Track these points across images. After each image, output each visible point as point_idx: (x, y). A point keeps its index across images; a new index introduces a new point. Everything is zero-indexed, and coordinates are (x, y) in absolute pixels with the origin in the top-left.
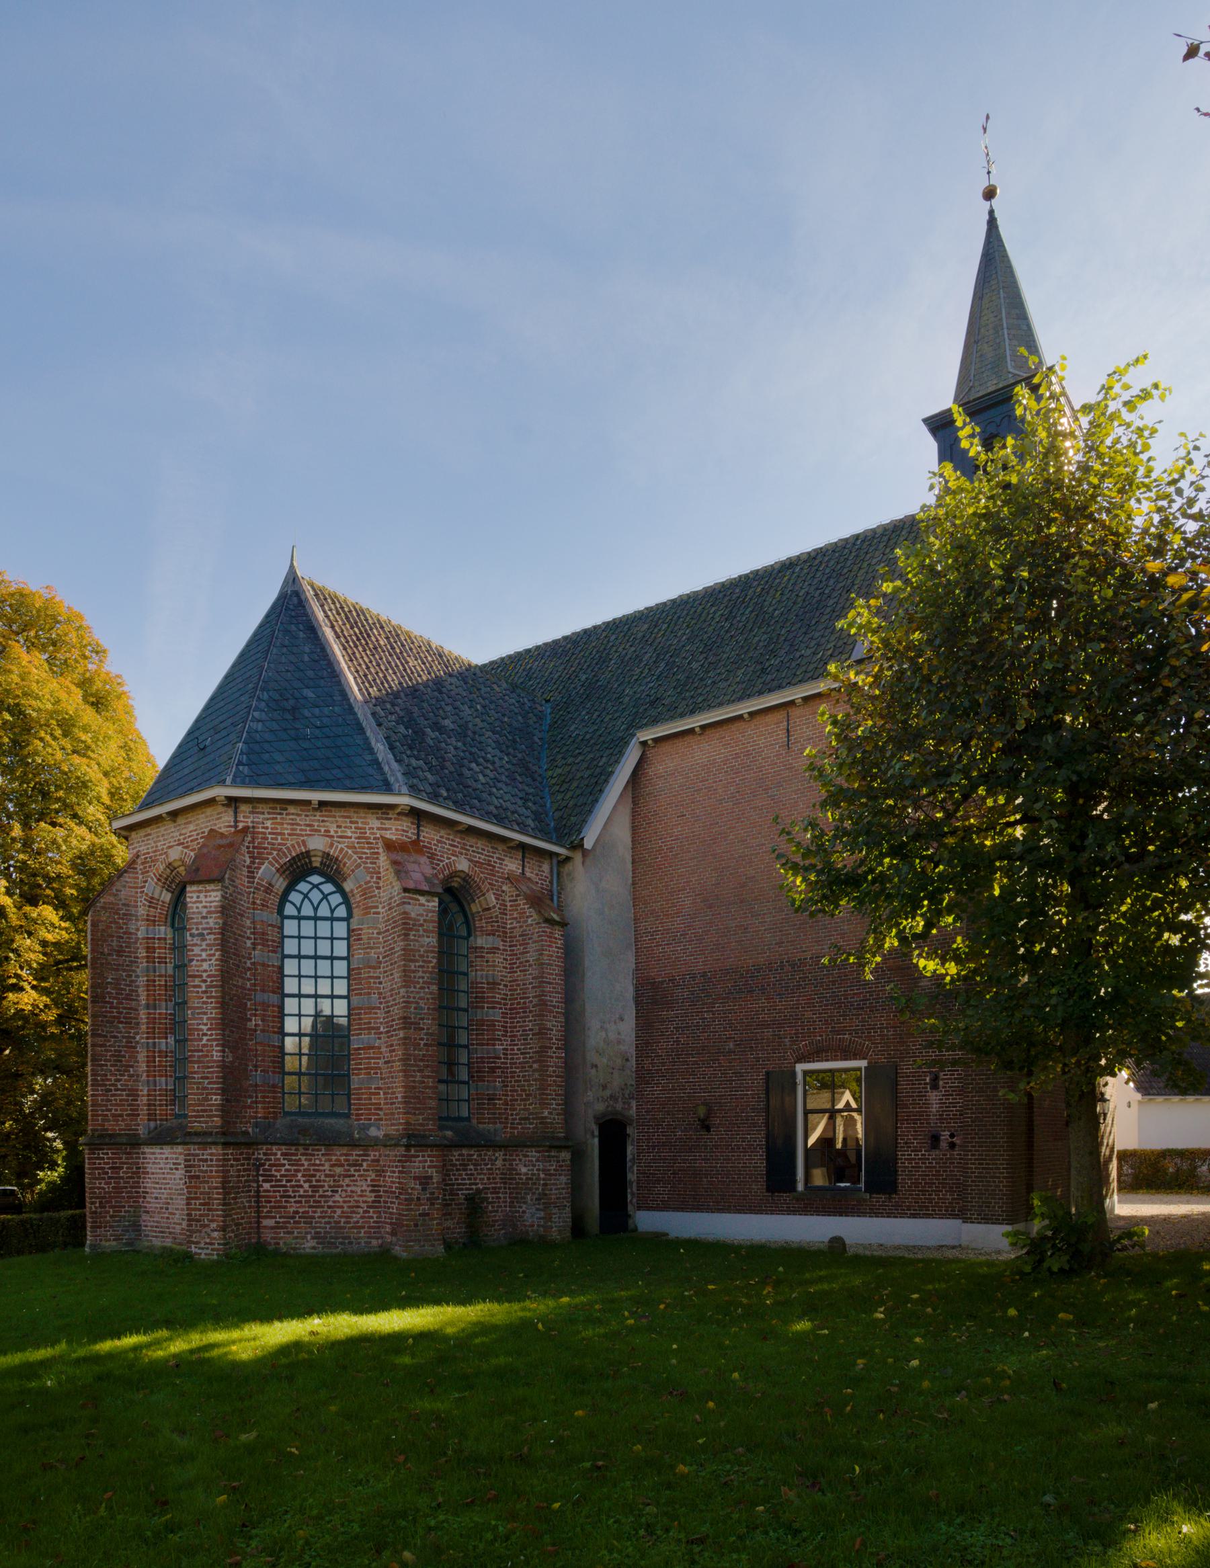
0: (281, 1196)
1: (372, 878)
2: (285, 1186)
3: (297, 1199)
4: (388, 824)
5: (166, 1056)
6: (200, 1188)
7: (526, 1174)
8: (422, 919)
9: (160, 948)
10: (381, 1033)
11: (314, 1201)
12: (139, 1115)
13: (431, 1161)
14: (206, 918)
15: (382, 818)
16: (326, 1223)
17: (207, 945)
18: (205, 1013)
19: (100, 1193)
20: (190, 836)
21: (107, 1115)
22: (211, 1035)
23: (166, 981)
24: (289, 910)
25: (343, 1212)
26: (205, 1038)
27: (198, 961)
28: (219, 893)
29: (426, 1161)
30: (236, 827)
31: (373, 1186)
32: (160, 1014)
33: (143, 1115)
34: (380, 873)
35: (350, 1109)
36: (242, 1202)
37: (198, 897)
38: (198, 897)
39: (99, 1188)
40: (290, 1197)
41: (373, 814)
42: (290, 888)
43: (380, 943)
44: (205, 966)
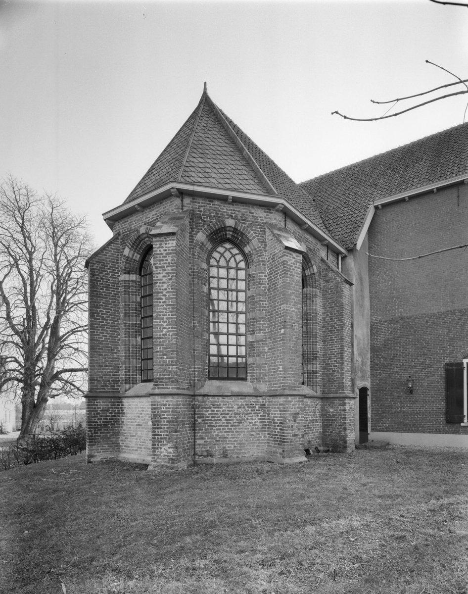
0: (208, 426)
1: (262, 245)
2: (211, 420)
3: (218, 427)
4: (271, 216)
5: (136, 348)
6: (161, 422)
7: (333, 412)
8: (294, 266)
9: (132, 286)
10: (267, 333)
11: (228, 429)
12: (119, 381)
13: (299, 405)
14: (165, 257)
15: (267, 212)
16: (234, 441)
17: (166, 273)
18: (165, 315)
19: (95, 425)
20: (152, 218)
21: (100, 380)
22: (169, 328)
23: (136, 305)
24: (213, 262)
25: (244, 435)
26: (165, 330)
27: (160, 283)
28: (174, 242)
29: (295, 405)
30: (182, 209)
31: (261, 419)
32: (132, 324)
33: (122, 381)
34: (266, 242)
35: (247, 376)
36: (186, 430)
37: (161, 244)
38: (161, 244)
39: (93, 422)
40: (214, 426)
41: (262, 209)
42: (214, 249)
43: (266, 282)
44: (165, 286)
